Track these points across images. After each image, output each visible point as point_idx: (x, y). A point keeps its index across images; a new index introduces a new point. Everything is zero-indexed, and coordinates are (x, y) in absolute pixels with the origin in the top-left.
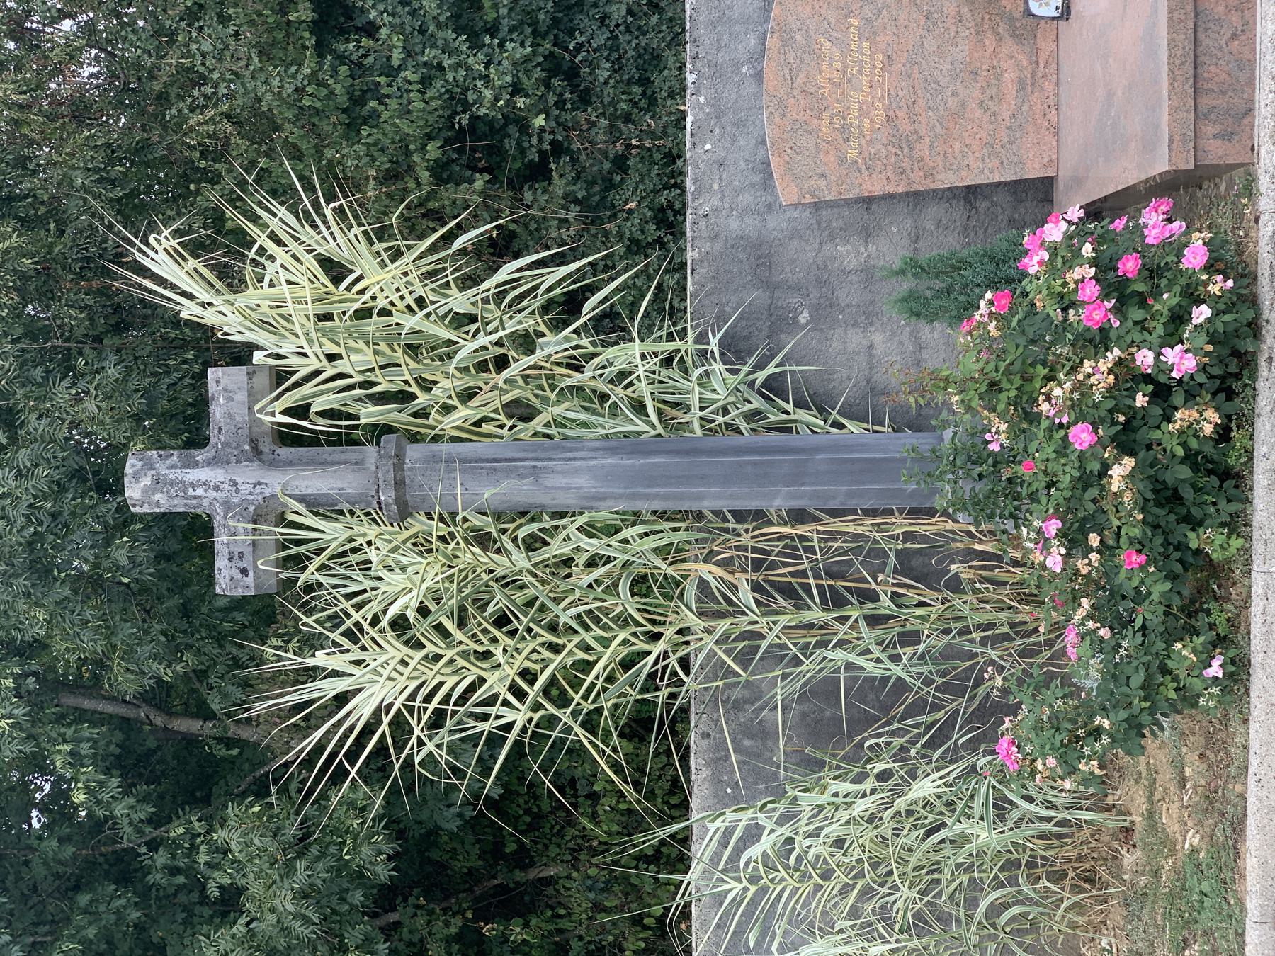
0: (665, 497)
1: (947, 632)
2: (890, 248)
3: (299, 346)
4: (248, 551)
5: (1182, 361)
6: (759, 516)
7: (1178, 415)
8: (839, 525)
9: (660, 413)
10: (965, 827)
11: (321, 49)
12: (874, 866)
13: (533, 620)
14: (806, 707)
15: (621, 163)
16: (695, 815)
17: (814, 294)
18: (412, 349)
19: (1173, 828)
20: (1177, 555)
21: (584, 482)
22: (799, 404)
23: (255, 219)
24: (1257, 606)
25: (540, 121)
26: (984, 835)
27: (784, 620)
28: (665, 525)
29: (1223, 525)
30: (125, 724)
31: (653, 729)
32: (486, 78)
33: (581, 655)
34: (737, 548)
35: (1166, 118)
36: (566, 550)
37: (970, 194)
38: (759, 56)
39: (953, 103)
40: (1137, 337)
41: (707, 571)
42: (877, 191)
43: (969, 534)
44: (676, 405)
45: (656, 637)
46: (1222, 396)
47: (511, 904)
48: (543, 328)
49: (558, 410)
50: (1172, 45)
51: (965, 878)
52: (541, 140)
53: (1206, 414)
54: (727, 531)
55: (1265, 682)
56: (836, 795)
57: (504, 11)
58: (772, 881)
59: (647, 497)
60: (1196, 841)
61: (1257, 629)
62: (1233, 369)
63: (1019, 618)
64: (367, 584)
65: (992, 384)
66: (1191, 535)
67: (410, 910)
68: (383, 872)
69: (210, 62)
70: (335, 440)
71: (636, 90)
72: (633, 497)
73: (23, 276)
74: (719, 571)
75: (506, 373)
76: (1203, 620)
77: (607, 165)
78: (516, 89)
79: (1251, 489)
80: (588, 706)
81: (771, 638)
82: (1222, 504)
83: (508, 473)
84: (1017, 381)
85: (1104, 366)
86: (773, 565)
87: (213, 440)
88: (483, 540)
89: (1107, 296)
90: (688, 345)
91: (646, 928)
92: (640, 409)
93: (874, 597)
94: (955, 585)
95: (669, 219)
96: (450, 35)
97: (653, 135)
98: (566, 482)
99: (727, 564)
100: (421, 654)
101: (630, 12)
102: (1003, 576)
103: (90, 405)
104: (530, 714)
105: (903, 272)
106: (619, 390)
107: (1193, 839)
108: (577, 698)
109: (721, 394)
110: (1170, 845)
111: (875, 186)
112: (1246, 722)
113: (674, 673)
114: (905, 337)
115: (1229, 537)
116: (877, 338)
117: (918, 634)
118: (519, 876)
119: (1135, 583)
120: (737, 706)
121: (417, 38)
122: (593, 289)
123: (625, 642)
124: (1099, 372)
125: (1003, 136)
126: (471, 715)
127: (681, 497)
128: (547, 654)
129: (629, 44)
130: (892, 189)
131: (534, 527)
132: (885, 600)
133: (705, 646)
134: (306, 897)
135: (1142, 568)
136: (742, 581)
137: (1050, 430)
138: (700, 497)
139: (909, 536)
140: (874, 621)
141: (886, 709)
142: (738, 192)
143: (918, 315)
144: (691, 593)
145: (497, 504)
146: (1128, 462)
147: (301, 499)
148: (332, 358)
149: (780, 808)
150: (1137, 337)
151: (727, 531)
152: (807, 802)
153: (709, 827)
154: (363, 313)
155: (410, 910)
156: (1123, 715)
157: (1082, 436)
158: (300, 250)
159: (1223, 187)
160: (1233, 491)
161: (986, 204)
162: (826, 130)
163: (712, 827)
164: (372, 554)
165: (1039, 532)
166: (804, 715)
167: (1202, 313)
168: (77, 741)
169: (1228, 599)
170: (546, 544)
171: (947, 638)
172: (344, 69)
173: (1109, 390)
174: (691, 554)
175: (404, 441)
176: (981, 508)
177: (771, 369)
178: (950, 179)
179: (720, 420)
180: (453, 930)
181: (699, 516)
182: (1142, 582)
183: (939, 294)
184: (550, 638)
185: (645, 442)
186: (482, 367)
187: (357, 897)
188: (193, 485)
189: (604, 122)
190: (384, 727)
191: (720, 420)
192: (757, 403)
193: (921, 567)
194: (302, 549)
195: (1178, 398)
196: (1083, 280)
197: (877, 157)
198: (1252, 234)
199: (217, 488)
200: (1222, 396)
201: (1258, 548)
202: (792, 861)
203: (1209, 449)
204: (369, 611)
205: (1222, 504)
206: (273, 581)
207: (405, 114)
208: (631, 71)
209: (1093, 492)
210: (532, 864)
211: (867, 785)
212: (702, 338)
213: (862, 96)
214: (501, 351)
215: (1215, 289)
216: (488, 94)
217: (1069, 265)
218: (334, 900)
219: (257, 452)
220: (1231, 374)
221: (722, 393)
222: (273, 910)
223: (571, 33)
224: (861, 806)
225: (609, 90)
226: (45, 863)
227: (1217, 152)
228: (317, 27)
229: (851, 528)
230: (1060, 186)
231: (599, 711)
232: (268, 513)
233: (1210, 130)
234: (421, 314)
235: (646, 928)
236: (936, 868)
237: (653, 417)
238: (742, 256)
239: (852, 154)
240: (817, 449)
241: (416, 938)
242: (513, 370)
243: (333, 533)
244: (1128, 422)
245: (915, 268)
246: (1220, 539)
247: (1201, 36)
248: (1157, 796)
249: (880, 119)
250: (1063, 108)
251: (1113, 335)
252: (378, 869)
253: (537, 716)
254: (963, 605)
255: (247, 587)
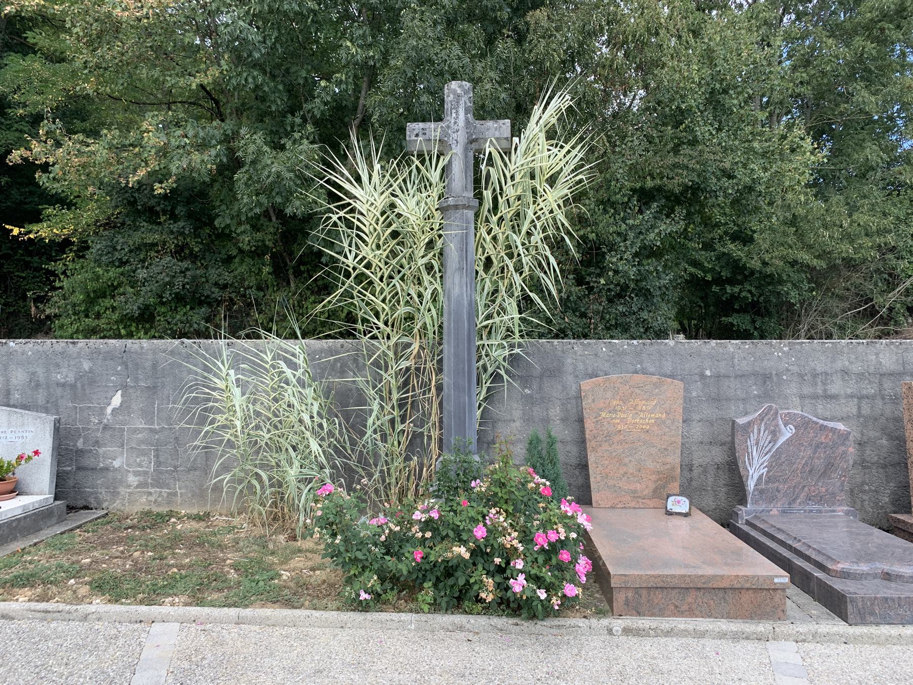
0: (449, 328)
1: (387, 455)
2: (560, 431)
3: (518, 162)
4: (427, 137)
5: (519, 584)
6: (440, 370)
7: (490, 580)
8: (435, 406)
9: (486, 327)
10: (297, 464)
11: (634, 190)
12: (280, 422)
13: (394, 267)
14: (354, 391)
15: (583, 315)
16: (303, 341)
17: (538, 396)
18: (518, 214)
19: (293, 564)
20: (420, 576)
21: (456, 291)
22: (489, 389)
23: (577, 144)
24: (395, 616)
25: (602, 281)
26: (292, 473)
27: (393, 381)
28: (436, 328)
29: (435, 600)
30: (355, 109)
31: (345, 324)
32: (621, 259)
33: (378, 289)
34: (426, 361)
35: (636, 573)
36: (426, 283)
37: (584, 466)
38: (644, 372)
39: (626, 460)
40: (529, 559)
41: (415, 347)
42: (586, 426)
43: (431, 465)
44: (490, 333)
45: (386, 323)
46: (499, 601)
47: (279, 270)
48: (524, 275)
49: (487, 280)
50: (673, 576)
51: (274, 464)
52: (596, 282)
53: (491, 594)
54: (433, 356)
55: (357, 621)
56: (312, 404)
57: (647, 268)
58: (273, 374)
59: (449, 319)
60: (284, 577)
61: (383, 616)
62: (512, 605)
63: (393, 488)
64: (411, 192)
65: (503, 484)
66: (430, 584)
67: (276, 226)
68: (289, 211)
69: (629, 144)
70: (477, 181)
71: (613, 322)
72: (449, 314)
73: (542, 63)
74: (415, 352)
75: (506, 258)
76: (388, 585)
77: (583, 310)
78: (616, 272)
79: (452, 613)
80: (355, 293)
81: (385, 375)
82: (445, 599)
83: (461, 257)
84: (506, 497)
85: (515, 542)
86: (418, 377)
87: (477, 122)
88: (430, 245)
89: (550, 544)
90: (517, 339)
91: (268, 323)
92: (489, 317)
93: (403, 421)
94: (407, 459)
95: (562, 334)
96: (639, 245)
97: (595, 329)
98: (457, 283)
99: (418, 356)
100: (378, 215)
101: (645, 320)
102: (411, 481)
103: (488, 86)
104: (352, 266)
105: (550, 437)
106: (497, 308)
107: (286, 575)
108: (359, 288)
109: (494, 354)
110: (285, 561)
111: (589, 425)
112: (338, 609)
113: (370, 332)
114: (518, 436)
115: (429, 604)
116: (518, 424)
117: (386, 442)
118: (291, 271)
119: (407, 555)
120: (355, 361)
121: (638, 231)
122: (543, 299)
123: (384, 309)
124: (512, 540)
125: (611, 483)
126: (351, 240)
127: (449, 335)
128: (379, 275)
129: (631, 319)
130: (587, 432)
131: (436, 268)
132: (401, 427)
133: (382, 346)
134: (278, 177)
135: (414, 560)
136: (410, 363)
137: (482, 513)
138: (449, 343)
139: (430, 437)
140: (392, 422)
141: (353, 427)
142: (584, 362)
143: (530, 444)
144: (405, 340)
145: (447, 251)
146: (467, 556)
147: (450, 162)
148: (513, 178)
149: (306, 378)
150: (529, 559)
151: (433, 356)
152: (309, 392)
153: (297, 347)
154: (534, 192)
155: (276, 226)
156: (342, 549)
157: (480, 532)
158: (562, 164)
159: (597, 595)
160: (451, 603)
161: (578, 474)
162: (615, 403)
163: (297, 348)
164: (424, 195)
165: (432, 508)
166: (351, 390)
167: (542, 594)
168: (347, 84)
169: (398, 599)
170: (429, 274)
171: (383, 455)
172: (626, 199)
173: (503, 545)
174: (423, 340)
175: (476, 210)
176: (443, 474)
177: (505, 377)
178: (592, 458)
179: (483, 353)
180: (267, 243)
181: (440, 344)
182: (407, 558)
183: (539, 453)
184: (386, 276)
185: (474, 320)
186: (509, 247)
187: (279, 200)
188: (457, 112)
189: (601, 308)
190: (348, 200)
191: (483, 353)
192: (490, 370)
193: (416, 443)
194: (427, 162)
195: (498, 579)
196: (558, 533)
197: (602, 426)
198: (578, 614)
199: (455, 123)
200: (499, 601)
201: (423, 617)
202: (282, 384)
203: (472, 593)
204: (398, 192)
205: (445, 599)
206: (413, 149)
207: (607, 225)
208: (621, 320)
209: (451, 534)
210: (296, 277)
211: (317, 419)
212: (520, 345)
213: (630, 419)
214: (516, 255)
215: (554, 600)
216: (615, 260)
217: (566, 526)
218: (277, 190)
219: (472, 142)
220: (512, 607)
221: (495, 354)
222: (272, 163)
223: (636, 295)
224: (306, 418)
225: (614, 311)
226: (296, 71)
227: (619, 598)
228: (642, 189)
229: (433, 412)
230: (589, 509)
231: (353, 298)
232: (444, 147)
233: (630, 594)
234: (534, 217)
235: (268, 323)
236: (279, 449)
237: (485, 323)
238: (555, 364)
239: (603, 415)
240: (470, 397)
241: (264, 228)
242: (507, 261)
243: (434, 176)
244: (487, 554)
245: (552, 443)
246: (429, 599)
247: (677, 591)
248: (308, 554)
249: (619, 427)
250: (624, 511)
251: (530, 546)
252: (290, 208)
253: (350, 269)
254: (398, 463)
255: (410, 136)
